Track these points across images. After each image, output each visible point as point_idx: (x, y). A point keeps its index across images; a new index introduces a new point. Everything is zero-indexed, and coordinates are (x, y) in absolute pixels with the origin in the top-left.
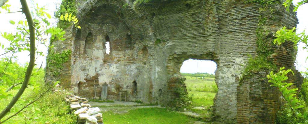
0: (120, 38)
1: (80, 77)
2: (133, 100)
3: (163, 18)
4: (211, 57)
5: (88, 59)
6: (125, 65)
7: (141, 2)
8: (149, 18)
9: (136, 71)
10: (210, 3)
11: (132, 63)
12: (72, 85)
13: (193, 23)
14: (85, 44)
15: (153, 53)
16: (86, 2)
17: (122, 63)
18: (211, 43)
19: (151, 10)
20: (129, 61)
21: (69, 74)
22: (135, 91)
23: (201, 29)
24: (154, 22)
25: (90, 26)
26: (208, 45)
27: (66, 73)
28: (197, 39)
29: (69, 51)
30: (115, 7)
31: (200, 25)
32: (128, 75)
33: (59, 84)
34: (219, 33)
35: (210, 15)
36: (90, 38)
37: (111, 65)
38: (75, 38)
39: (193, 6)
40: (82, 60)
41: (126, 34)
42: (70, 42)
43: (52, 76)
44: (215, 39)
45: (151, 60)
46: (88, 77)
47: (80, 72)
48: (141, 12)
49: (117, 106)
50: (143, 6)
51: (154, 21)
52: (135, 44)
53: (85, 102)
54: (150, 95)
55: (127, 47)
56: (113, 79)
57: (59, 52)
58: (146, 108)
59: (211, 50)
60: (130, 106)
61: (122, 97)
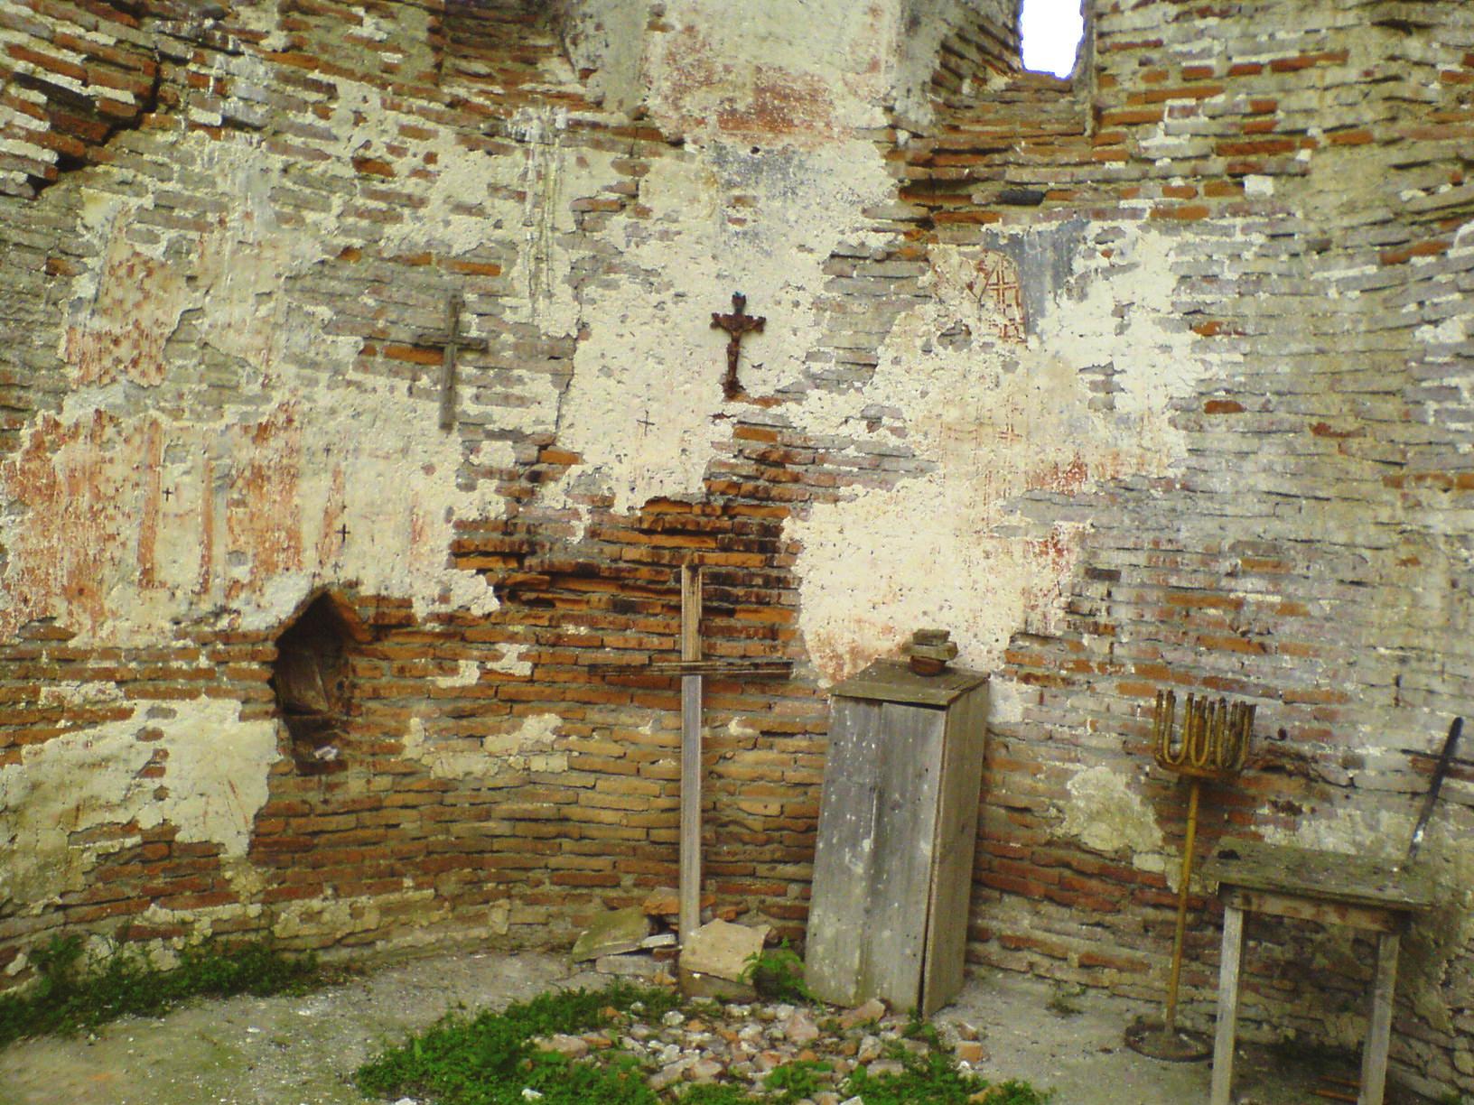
37: (1064, 251)
46: (553, 496)
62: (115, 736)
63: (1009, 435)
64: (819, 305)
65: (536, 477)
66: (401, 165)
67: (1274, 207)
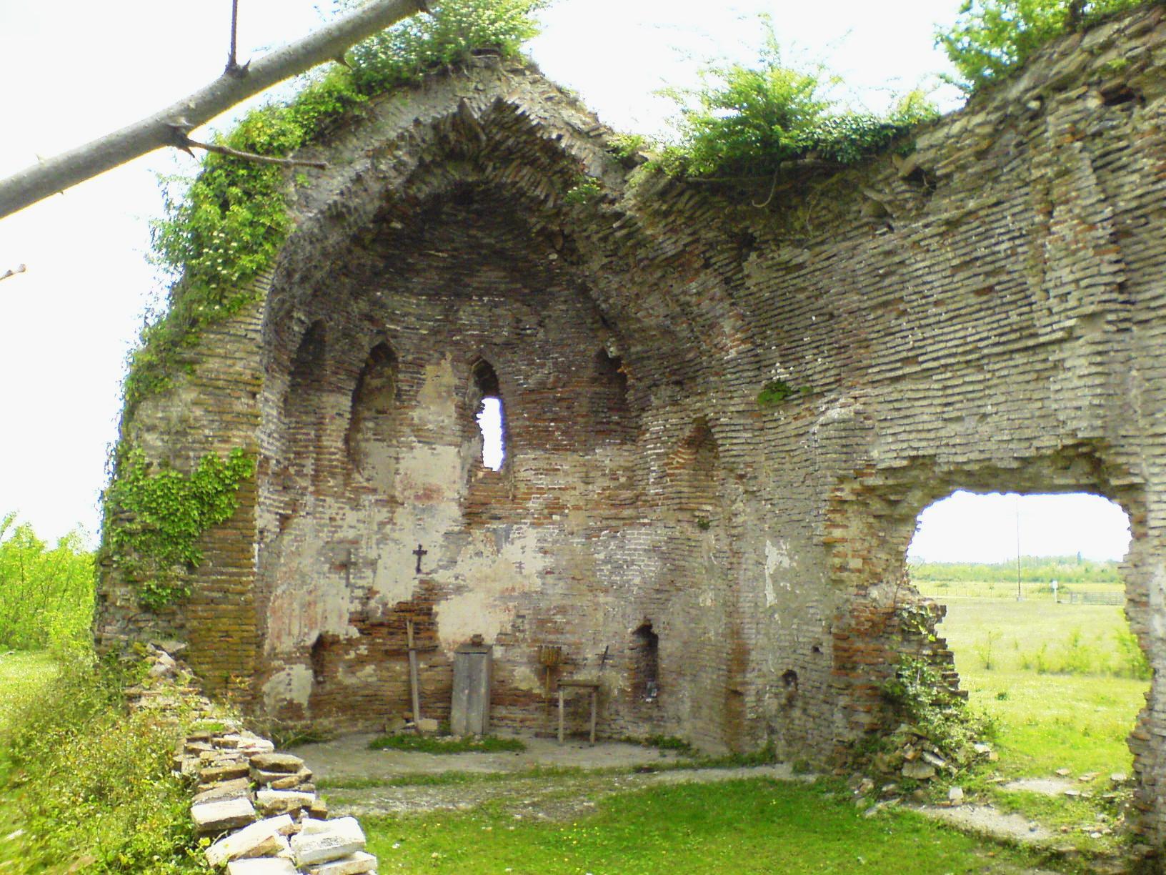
0: (558, 379)
1: (319, 608)
2: (634, 735)
3: (800, 260)
4: (1087, 469)
5: (372, 498)
6: (590, 534)
7: (670, 174)
8: (719, 259)
9: (652, 567)
10: (1052, 144)
11: (632, 522)
12: (274, 654)
13: (960, 276)
14: (354, 411)
15: (748, 465)
16: (349, 172)
17: (575, 520)
18: (1081, 383)
19: (733, 218)
20: (613, 511)
21: (242, 593)
22: (649, 684)
23: (1014, 302)
24: (749, 283)
25: (383, 306)
26: (1060, 396)
27: (226, 591)
28: (991, 367)
29: (244, 456)
30: (523, 200)
31: (999, 283)
32: (606, 591)
33: (176, 660)
34: (1122, 315)
35: (1055, 214)
36: (380, 375)
37: (508, 532)
38: (288, 378)
39: (948, 176)
40: (332, 506)
41: (593, 351)
42: (251, 402)
43: (134, 610)
44: (1099, 353)
45: (739, 505)
46: (373, 603)
47: (322, 581)
48: (673, 231)
49: (536, 774)
50: (686, 196)
51: (748, 276)
52: (643, 410)
53: (293, 778)
54: (735, 703)
55: (599, 427)
56: (522, 612)
57: (178, 463)
58: (702, 782)
59: (1085, 428)
60: (612, 771)
61: (573, 715)
62: (282, 675)
63: (494, 581)
64: (441, 546)
65: (368, 598)
66: (338, 517)
67: (560, 523)
